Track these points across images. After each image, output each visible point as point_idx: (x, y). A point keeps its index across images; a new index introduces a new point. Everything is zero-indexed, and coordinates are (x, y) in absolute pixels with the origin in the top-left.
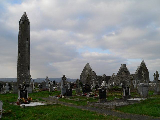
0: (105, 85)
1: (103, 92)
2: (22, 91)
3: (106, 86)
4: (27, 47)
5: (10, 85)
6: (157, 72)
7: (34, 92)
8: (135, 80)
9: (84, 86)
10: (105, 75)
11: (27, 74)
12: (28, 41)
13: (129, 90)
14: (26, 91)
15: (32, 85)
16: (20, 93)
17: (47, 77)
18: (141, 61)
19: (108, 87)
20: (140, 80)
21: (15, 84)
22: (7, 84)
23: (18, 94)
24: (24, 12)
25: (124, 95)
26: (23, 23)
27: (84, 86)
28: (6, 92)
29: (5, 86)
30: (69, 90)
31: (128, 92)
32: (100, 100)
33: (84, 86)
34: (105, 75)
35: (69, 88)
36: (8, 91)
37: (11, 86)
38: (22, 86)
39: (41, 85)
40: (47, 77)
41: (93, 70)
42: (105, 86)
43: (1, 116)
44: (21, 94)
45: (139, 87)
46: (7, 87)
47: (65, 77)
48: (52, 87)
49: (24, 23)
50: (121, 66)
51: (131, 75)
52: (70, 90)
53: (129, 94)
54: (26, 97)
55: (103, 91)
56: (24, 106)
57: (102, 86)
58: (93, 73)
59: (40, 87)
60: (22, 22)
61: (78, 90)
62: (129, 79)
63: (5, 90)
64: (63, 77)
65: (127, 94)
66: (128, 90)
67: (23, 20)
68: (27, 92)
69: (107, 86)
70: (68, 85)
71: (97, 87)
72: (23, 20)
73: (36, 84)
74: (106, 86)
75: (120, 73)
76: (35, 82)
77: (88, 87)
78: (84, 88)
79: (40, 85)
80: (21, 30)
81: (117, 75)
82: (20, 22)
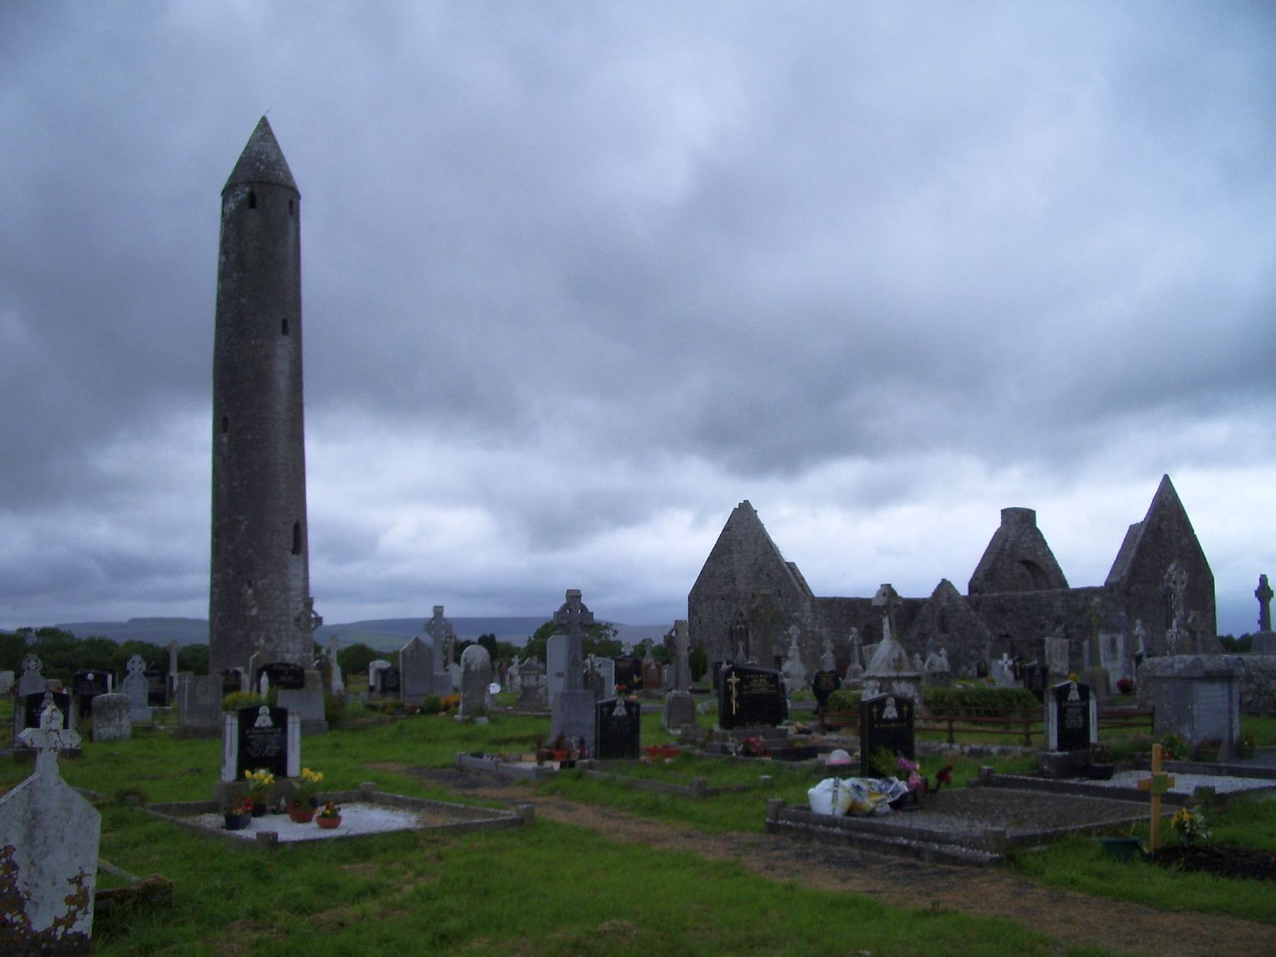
0: (898, 668)
1: (894, 720)
2: (247, 716)
3: (899, 679)
4: (282, 382)
5: (158, 663)
6: (1263, 580)
7: (335, 718)
8: (1110, 628)
9: (728, 674)
10: (888, 591)
11: (286, 589)
12: (286, 340)
13: (1092, 704)
14: (280, 717)
15: (325, 669)
16: (236, 728)
17: (438, 611)
18: (1150, 490)
19: (916, 680)
20: (1144, 627)
21: (194, 661)
22: (137, 665)
23: (217, 733)
24: (261, 117)
25: (1053, 743)
26: (252, 201)
27: (734, 679)
28: (126, 723)
29: (121, 672)
30: (612, 705)
31: (1081, 720)
32: (1173, 786)
33: (728, 674)
34: (888, 591)
35: (611, 689)
36: (144, 713)
37: (163, 681)
38: (246, 679)
39: (396, 672)
40: (438, 611)
41: (788, 555)
42: (893, 674)
43: (91, 916)
44: (244, 742)
45: (1165, 686)
46: (136, 687)
47: (584, 608)
48: (476, 680)
49: (259, 200)
50: (995, 523)
51: (1077, 592)
52: (620, 711)
53: (1093, 739)
54: (278, 764)
55: (890, 712)
56: (270, 841)
57: (868, 678)
58: (788, 578)
59: (385, 690)
60: (243, 193)
61: (681, 711)
62: (1058, 621)
63: (119, 706)
64: (564, 608)
65: (1073, 737)
66: (1085, 712)
67: (249, 183)
68: (290, 727)
69: (908, 679)
70: (603, 672)
71: (824, 687)
72: (249, 183)
73: (356, 660)
74: (899, 679)
75: (937, 593)
76: (344, 646)
77: (760, 686)
78: (728, 694)
79: (383, 673)
80: (233, 256)
81: (963, 590)
82: (228, 192)
